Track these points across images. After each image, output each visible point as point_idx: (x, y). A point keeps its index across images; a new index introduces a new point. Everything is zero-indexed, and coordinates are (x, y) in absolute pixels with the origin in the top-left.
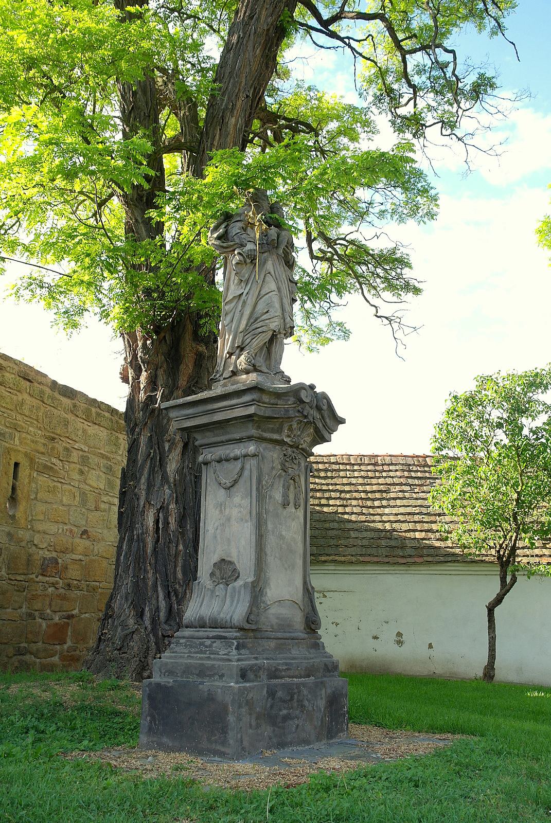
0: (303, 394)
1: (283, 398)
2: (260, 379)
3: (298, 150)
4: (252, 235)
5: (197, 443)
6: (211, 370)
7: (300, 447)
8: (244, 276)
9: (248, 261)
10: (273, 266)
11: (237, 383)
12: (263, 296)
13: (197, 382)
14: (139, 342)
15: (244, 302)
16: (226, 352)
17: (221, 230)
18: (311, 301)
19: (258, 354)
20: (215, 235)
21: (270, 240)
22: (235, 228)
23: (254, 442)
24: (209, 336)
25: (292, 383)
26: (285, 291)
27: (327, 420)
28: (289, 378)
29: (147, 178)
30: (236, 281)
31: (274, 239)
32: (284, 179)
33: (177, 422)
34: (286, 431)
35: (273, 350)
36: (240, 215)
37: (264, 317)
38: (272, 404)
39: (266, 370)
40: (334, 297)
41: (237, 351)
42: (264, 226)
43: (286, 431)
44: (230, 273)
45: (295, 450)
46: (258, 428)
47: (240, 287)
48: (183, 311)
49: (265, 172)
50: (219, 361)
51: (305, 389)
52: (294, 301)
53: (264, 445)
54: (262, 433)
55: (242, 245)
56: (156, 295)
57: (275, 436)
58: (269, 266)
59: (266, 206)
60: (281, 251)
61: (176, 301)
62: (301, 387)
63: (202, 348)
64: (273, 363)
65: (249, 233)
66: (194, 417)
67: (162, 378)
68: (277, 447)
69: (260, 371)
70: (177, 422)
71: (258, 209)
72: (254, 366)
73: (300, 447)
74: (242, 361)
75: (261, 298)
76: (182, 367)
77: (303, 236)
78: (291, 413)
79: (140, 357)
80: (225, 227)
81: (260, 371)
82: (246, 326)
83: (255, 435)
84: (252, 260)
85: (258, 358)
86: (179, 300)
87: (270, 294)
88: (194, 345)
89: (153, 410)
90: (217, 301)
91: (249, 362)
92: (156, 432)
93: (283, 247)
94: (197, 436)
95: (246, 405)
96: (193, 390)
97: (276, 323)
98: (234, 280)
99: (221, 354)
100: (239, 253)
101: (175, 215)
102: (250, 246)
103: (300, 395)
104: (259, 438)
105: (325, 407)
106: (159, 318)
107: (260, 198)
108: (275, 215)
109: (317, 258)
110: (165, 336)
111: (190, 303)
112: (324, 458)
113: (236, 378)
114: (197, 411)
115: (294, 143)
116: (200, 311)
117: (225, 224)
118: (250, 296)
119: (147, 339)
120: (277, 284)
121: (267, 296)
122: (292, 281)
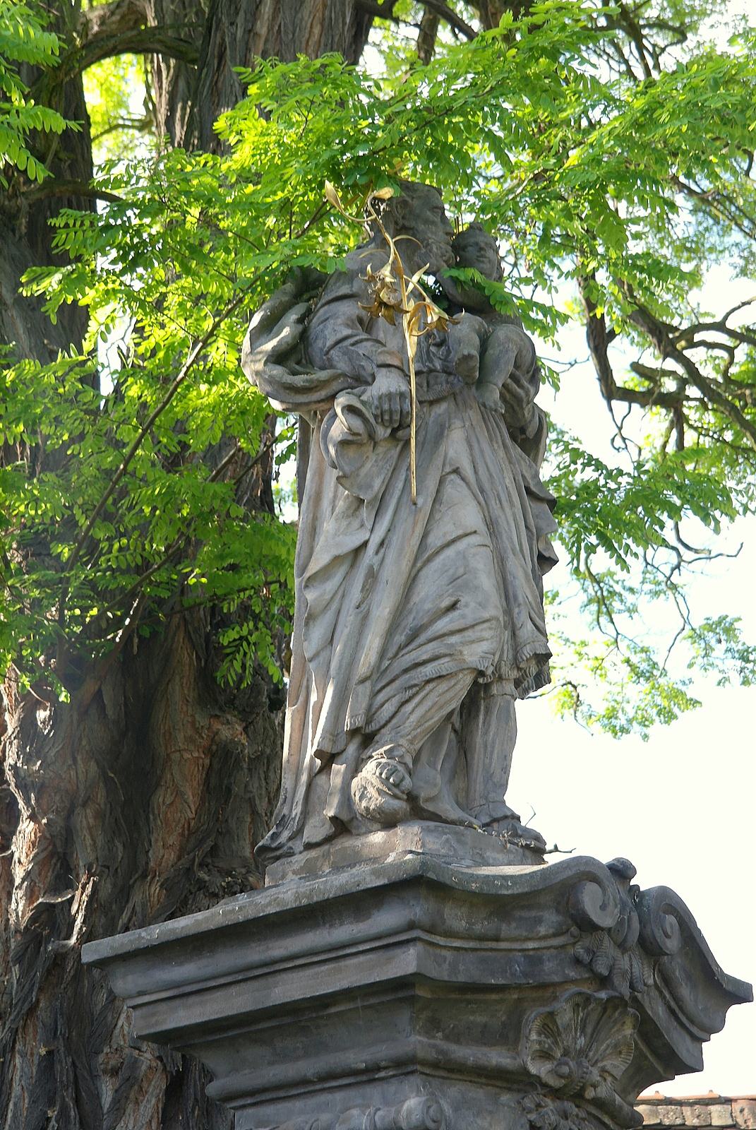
0: (590, 900)
1: (518, 914)
2: (435, 844)
3: (544, 52)
4: (392, 344)
5: (212, 1089)
6: (262, 806)
7: (590, 1094)
8: (370, 486)
9: (382, 432)
10: (471, 447)
11: (354, 859)
12: (437, 553)
13: (214, 851)
14: (7, 716)
15: (372, 576)
16: (310, 751)
17: (286, 331)
18: (610, 547)
19: (424, 758)
20: (269, 346)
21: (455, 357)
22: (334, 324)
23: (416, 1080)
24: (254, 688)
25: (551, 859)
26: (511, 518)
27: (685, 991)
28: (538, 838)
29: (36, 142)
30: (341, 504)
31: (470, 357)
32: (497, 147)
33: (146, 1008)
34: (534, 1036)
35: (479, 740)
36: (348, 276)
37: (442, 625)
38: (481, 938)
39: (453, 812)
40: (691, 524)
41: (352, 749)
42: (434, 314)
43: (534, 1036)
44: (320, 475)
45: (569, 1106)
46: (433, 1025)
47: (356, 524)
48: (160, 602)
49: (433, 128)
50: (287, 782)
51: (594, 879)
52: (546, 562)
53: (455, 1090)
54: (445, 1045)
55: (360, 380)
56: (65, 552)
57: (497, 1057)
58: (456, 446)
59: (438, 243)
60: (494, 395)
61: (139, 570)
62: (583, 872)
63: (231, 730)
64: (478, 787)
65: (381, 336)
66: (202, 989)
67: (89, 842)
68: (505, 1098)
69: (435, 817)
70: (146, 1008)
71: (412, 257)
72: (412, 798)
73: (590, 1094)
74: (370, 782)
75: (429, 560)
76: (162, 798)
77: (574, 336)
78: (551, 969)
79: (14, 768)
80: (300, 321)
81: (435, 817)
82: (382, 655)
83: (421, 1054)
84: (394, 431)
85: (425, 771)
86: (147, 564)
87: (461, 545)
88: (202, 721)
89: (59, 959)
90: (280, 564)
91: (393, 787)
92: (68, 1040)
93: (500, 378)
94: (212, 1060)
95: (388, 943)
96: (200, 881)
97: (485, 646)
98: (335, 497)
99: (294, 758)
100: (350, 409)
101: (127, 279)
102: (386, 383)
103: (578, 902)
104: (435, 1065)
105: (672, 944)
106: (78, 629)
107: (417, 217)
108: (472, 273)
109: (628, 395)
110: (99, 693)
111: (187, 575)
112: (687, 1111)
113: (346, 843)
114: (209, 971)
115: (534, 28)
116: (224, 598)
117: (299, 309)
118: (391, 554)
119: (37, 705)
120: (485, 507)
121: (450, 552)
122: (534, 494)
